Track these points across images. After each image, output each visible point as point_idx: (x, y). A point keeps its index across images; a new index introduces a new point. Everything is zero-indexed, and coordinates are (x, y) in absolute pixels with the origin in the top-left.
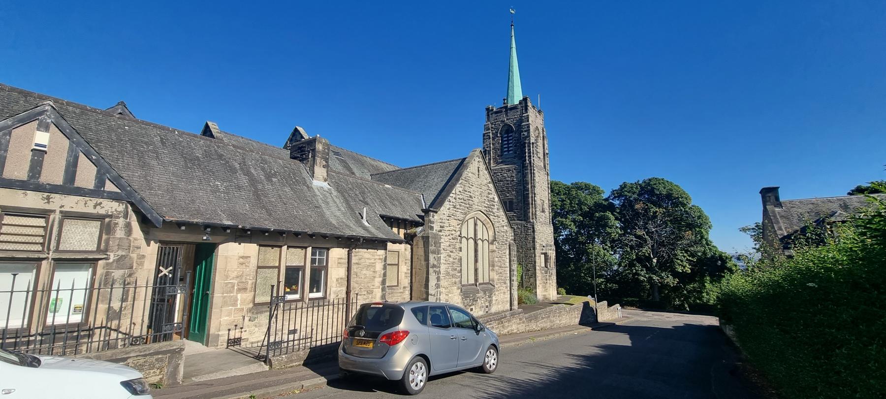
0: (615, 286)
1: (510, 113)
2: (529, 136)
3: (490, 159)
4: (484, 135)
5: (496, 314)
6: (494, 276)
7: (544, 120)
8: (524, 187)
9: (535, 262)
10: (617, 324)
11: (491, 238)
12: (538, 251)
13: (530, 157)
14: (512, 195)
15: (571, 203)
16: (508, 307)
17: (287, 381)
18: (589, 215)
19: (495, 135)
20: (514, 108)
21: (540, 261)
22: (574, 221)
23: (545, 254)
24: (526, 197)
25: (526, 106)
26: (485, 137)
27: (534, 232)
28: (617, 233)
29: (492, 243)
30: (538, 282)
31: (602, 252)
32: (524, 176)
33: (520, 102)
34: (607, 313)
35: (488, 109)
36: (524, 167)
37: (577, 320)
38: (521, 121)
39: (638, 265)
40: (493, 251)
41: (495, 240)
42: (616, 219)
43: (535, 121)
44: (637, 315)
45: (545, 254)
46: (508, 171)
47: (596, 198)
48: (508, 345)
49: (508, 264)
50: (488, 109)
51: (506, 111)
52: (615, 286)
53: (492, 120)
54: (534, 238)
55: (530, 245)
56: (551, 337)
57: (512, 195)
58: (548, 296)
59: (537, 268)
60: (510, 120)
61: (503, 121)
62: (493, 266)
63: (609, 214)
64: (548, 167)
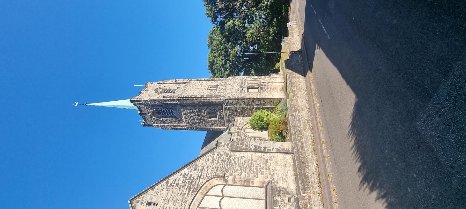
0: (275, 20)
1: (144, 111)
2: (158, 101)
3: (179, 126)
4: (163, 129)
5: (297, 183)
6: (258, 181)
7: (152, 81)
8: (196, 104)
9: (254, 99)
10: (303, 33)
11: (222, 182)
12: (246, 95)
13: (173, 100)
14: (204, 113)
15: (221, 50)
16: (289, 157)
17: (315, 108)
18: (228, 39)
19: (162, 122)
20: (140, 109)
21: (254, 94)
22: (233, 48)
23: (248, 88)
24: (204, 104)
25: (137, 101)
26: (163, 128)
27: (230, 99)
28: (238, 21)
29: (226, 181)
30: (270, 97)
31: (252, 31)
32: (188, 104)
33: (135, 105)
34: (293, 42)
35: (144, 125)
36: (182, 105)
37: (301, 78)
38: (148, 105)
39: (260, 6)
40: (234, 180)
41: (223, 177)
42: (229, 21)
43: (150, 93)
44: (294, 8)
45: (248, 88)
46: (187, 116)
47: (217, 32)
48: (328, 169)
49: (250, 154)
50: (144, 125)
51: (143, 114)
52: (275, 20)
53: (151, 123)
54: (235, 99)
55: (241, 102)
56: (330, 173)
57: (204, 113)
58: (281, 87)
59: (258, 97)
60: (149, 114)
61: (151, 116)
62: (248, 181)
63: (226, 26)
64: (186, 80)
